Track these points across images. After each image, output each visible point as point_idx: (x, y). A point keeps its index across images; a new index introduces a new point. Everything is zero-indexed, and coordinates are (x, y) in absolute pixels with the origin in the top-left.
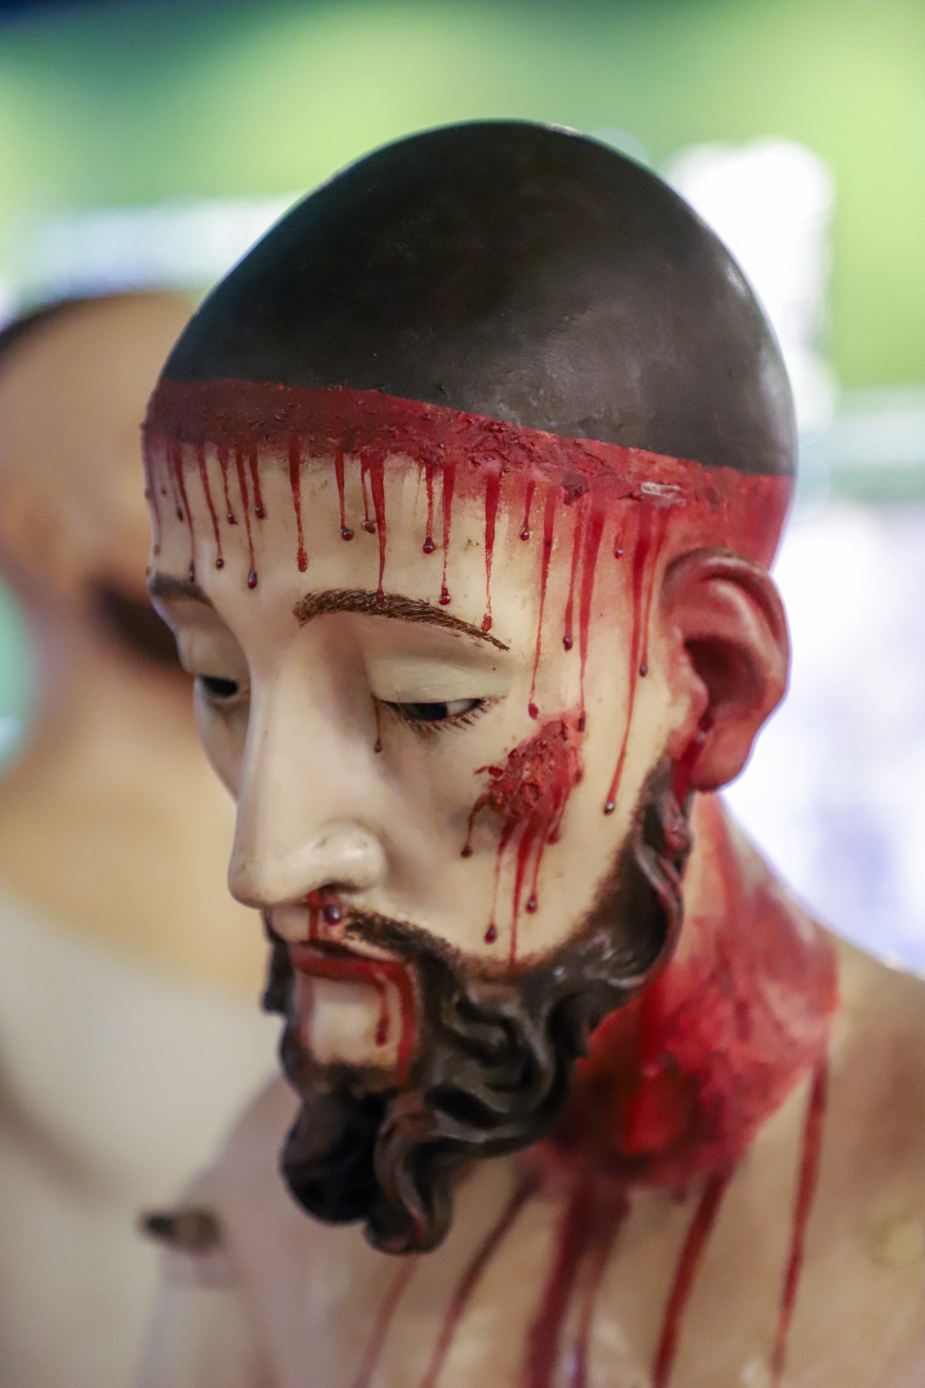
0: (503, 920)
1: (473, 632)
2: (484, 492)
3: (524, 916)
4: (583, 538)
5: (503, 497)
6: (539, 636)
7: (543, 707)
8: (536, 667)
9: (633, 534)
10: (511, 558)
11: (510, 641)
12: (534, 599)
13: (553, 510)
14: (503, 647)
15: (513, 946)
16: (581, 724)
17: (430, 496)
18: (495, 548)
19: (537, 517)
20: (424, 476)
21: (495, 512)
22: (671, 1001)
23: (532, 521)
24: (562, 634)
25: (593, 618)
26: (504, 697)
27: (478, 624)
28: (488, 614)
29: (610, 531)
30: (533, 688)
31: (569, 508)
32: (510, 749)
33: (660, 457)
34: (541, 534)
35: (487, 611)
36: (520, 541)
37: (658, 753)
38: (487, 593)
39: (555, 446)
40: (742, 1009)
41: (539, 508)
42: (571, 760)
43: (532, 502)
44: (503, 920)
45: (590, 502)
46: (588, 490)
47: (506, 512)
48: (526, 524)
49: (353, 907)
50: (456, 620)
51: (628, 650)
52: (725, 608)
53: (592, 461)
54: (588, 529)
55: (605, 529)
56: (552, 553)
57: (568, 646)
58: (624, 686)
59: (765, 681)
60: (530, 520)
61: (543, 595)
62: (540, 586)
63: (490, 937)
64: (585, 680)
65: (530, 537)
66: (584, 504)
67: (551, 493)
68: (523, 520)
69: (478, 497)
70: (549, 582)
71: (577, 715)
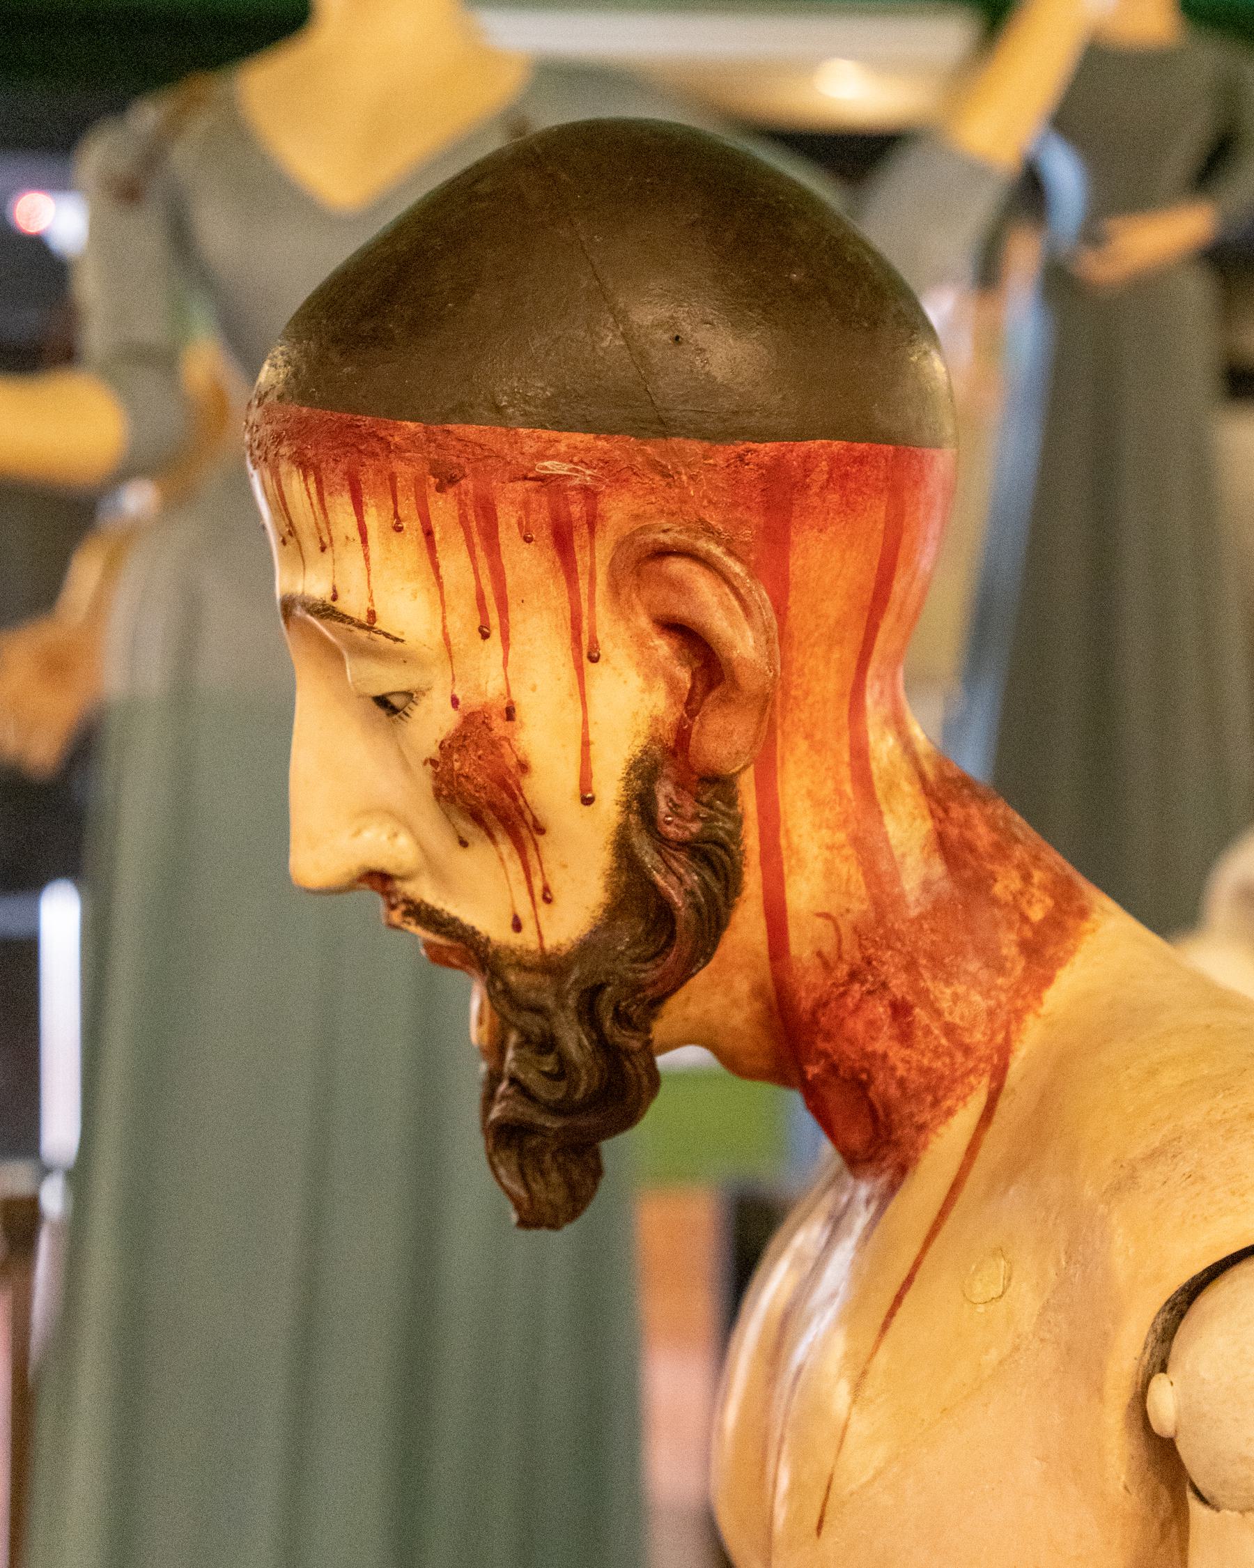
3: (543, 908)
6: (444, 627)
7: (463, 698)
8: (451, 657)
11: (402, 633)
14: (396, 640)
15: (541, 937)
16: (510, 713)
18: (370, 543)
19: (407, 508)
20: (302, 478)
22: (806, 1001)
23: (402, 512)
27: (363, 617)
28: (371, 608)
29: (508, 517)
30: (454, 679)
31: (444, 496)
32: (440, 740)
34: (417, 524)
35: (369, 604)
36: (394, 533)
37: (641, 741)
38: (369, 588)
40: (900, 1010)
42: (506, 749)
43: (398, 494)
44: (524, 911)
45: (471, 486)
46: (465, 476)
47: (372, 506)
48: (396, 515)
49: (405, 894)
51: (567, 639)
52: (678, 586)
54: (477, 516)
56: (436, 543)
57: (485, 636)
60: (399, 511)
61: (440, 585)
62: (433, 578)
65: (404, 528)
66: (462, 490)
67: (419, 482)
68: (392, 512)
69: (344, 494)
70: (442, 571)
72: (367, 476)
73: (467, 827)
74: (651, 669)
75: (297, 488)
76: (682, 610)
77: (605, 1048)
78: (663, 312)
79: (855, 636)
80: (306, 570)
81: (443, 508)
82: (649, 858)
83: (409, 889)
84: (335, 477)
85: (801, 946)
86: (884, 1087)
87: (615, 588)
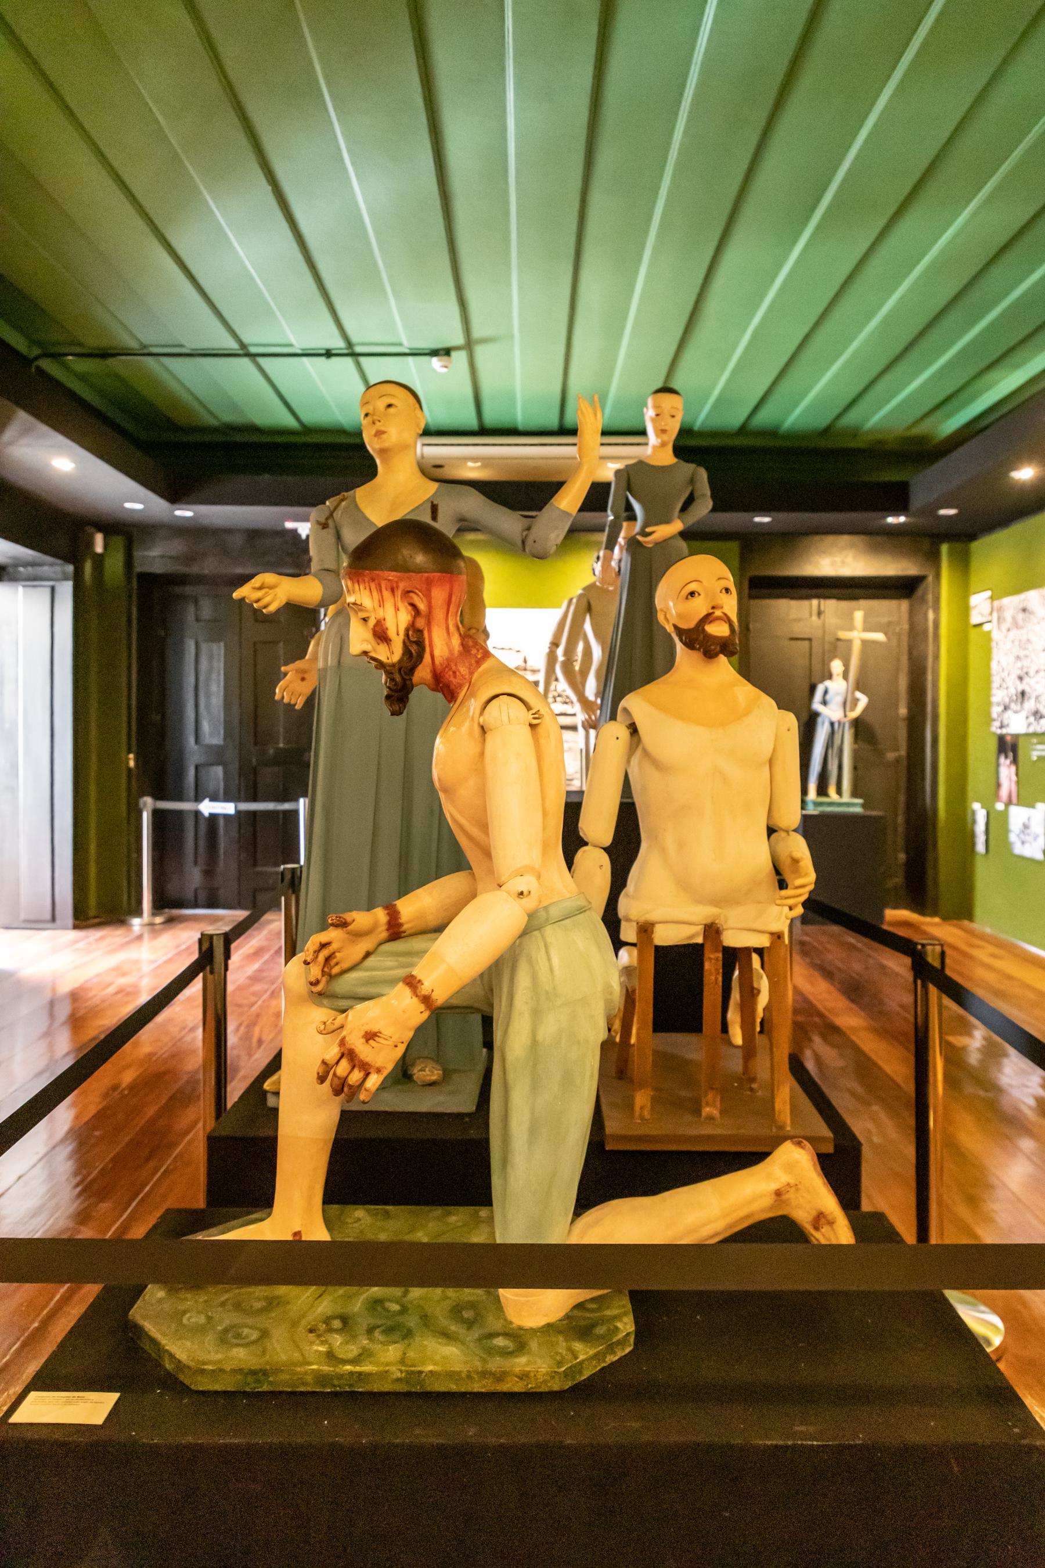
19: (367, 584)
40: (454, 673)
52: (411, 598)
58: (394, 612)
72: (360, 580)
73: (379, 641)
74: (408, 612)
75: (349, 583)
76: (412, 601)
77: (404, 680)
78: (409, 552)
79: (445, 607)
80: (771, 865)
81: (373, 585)
82: (408, 644)
83: (370, 654)
84: (355, 580)
85: (437, 662)
86: (452, 687)
87: (401, 598)
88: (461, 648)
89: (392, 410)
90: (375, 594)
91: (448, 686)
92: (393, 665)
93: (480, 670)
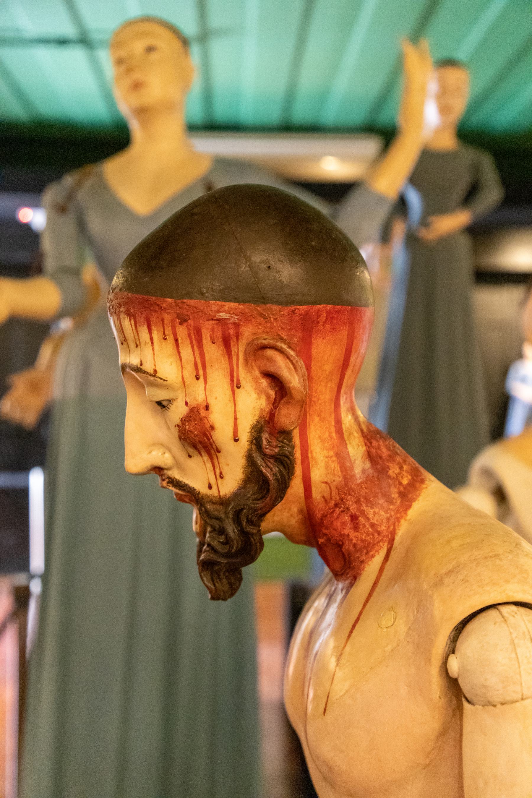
0: (213, 481)
1: (151, 375)
2: (146, 323)
4: (193, 337)
5: (153, 325)
9: (219, 334)
10: (162, 347)
11: (167, 378)
12: (176, 362)
13: (175, 328)
14: (164, 380)
16: (207, 408)
17: (132, 327)
18: (154, 344)
20: (129, 320)
21: (151, 331)
22: (318, 515)
23: (166, 333)
24: (195, 374)
25: (208, 367)
26: (177, 399)
27: (152, 372)
28: (155, 368)
29: (206, 334)
33: (228, 303)
35: (154, 367)
36: (163, 340)
38: (154, 361)
39: (173, 303)
40: (354, 518)
41: (168, 327)
42: (206, 421)
44: (213, 481)
45: (192, 323)
46: (190, 319)
47: (155, 330)
50: (145, 371)
51: (228, 379)
52: (270, 360)
53: (190, 307)
54: (194, 334)
55: (203, 333)
58: (229, 393)
59: (289, 388)
61: (181, 360)
62: (178, 357)
63: (210, 487)
64: (207, 391)
67: (173, 321)
70: (181, 355)
71: (205, 404)
72: (153, 319)
73: (191, 450)
74: (260, 391)
75: (127, 323)
76: (271, 369)
77: (243, 532)
78: (264, 257)
79: (336, 378)
81: (182, 331)
82: (259, 461)
83: (170, 473)
84: (141, 319)
85: (317, 494)
86: (348, 547)
87: (246, 360)
88: (368, 465)
89: (154, 56)
90: (187, 352)
91: (339, 546)
92: (223, 502)
93: (412, 513)
